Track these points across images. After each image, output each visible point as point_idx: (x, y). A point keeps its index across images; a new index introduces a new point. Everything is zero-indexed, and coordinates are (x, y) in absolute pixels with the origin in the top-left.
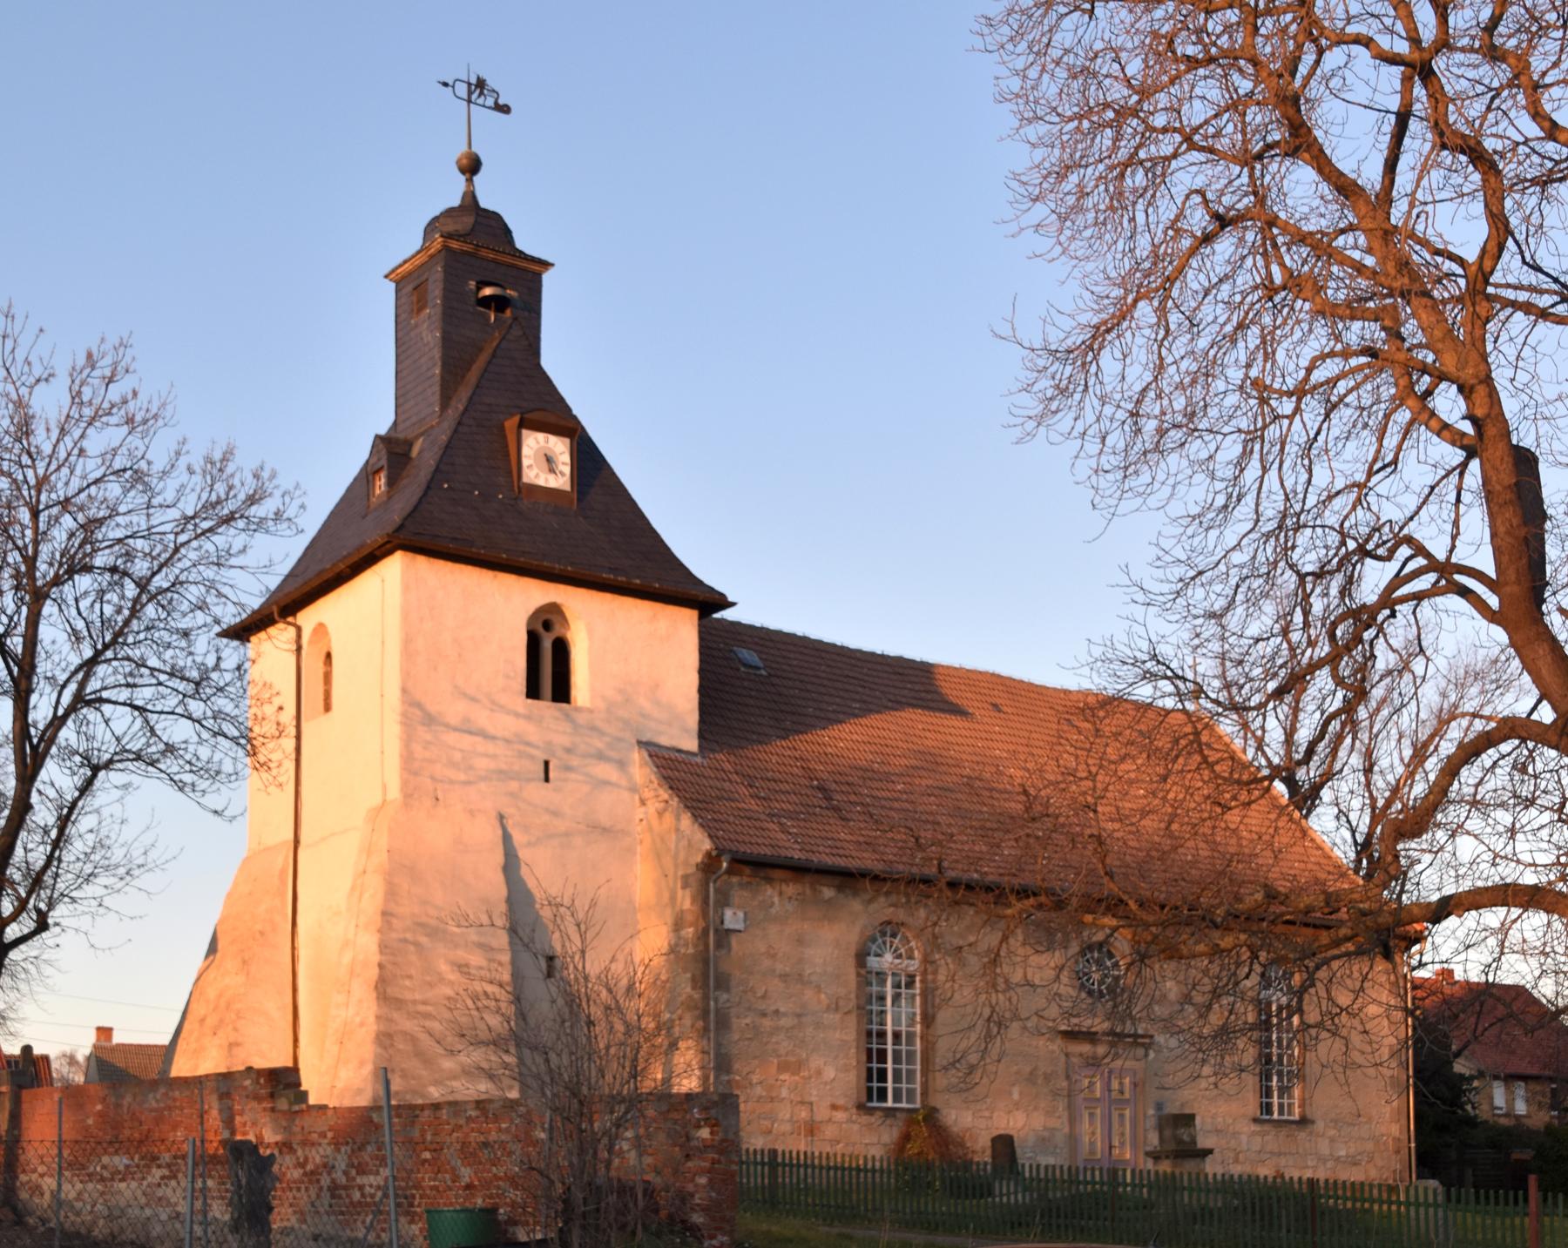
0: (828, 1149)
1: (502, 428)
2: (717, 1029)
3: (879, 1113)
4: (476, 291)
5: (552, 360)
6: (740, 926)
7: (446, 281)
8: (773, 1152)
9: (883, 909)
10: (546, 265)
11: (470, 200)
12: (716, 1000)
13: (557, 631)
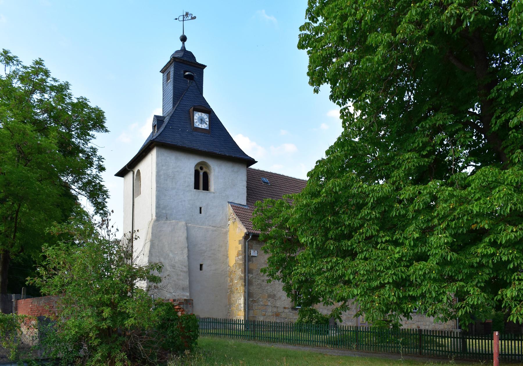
0: (283, 321)
1: (189, 111)
2: (248, 285)
4: (185, 73)
5: (206, 95)
6: (256, 255)
7: (174, 70)
8: (420, 331)
10: (205, 66)
11: (183, 49)
12: (248, 276)
13: (205, 170)
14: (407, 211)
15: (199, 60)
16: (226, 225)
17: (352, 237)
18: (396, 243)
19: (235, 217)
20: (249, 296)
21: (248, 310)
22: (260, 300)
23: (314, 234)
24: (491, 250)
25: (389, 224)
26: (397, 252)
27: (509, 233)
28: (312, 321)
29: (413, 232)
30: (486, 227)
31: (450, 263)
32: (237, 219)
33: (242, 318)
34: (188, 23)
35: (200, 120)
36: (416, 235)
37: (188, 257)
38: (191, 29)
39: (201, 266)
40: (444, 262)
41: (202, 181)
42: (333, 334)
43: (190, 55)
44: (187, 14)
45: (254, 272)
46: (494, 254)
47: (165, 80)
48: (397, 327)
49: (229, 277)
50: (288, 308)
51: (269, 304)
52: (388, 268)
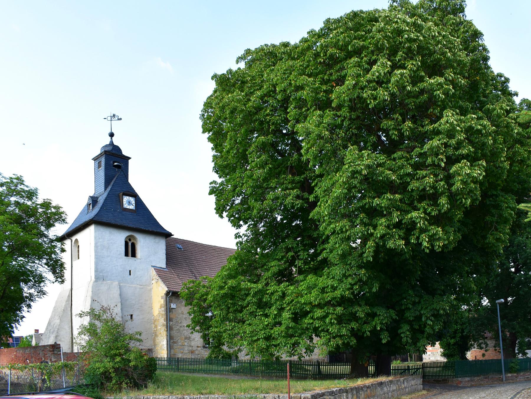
1: (119, 196)
4: (114, 163)
6: (175, 307)
10: (130, 158)
11: (112, 143)
13: (132, 241)
14: (271, 299)
15: (125, 153)
16: (150, 284)
17: (243, 311)
18: (266, 316)
19: (158, 278)
20: (171, 339)
21: (170, 349)
23: (222, 310)
24: (311, 321)
25: (262, 305)
26: (266, 321)
27: (318, 313)
28: (219, 356)
29: (274, 311)
30: (308, 310)
31: (291, 328)
32: (160, 280)
33: (166, 356)
34: (115, 123)
35: (128, 203)
36: (276, 312)
37: (121, 309)
38: (116, 127)
39: (131, 315)
40: (288, 328)
41: (130, 250)
42: (234, 365)
43: (117, 149)
44: (114, 116)
45: (173, 320)
46: (312, 323)
47: (97, 166)
48: (279, 359)
49: (154, 324)
50: (200, 347)
51: (186, 344)
52: (261, 330)
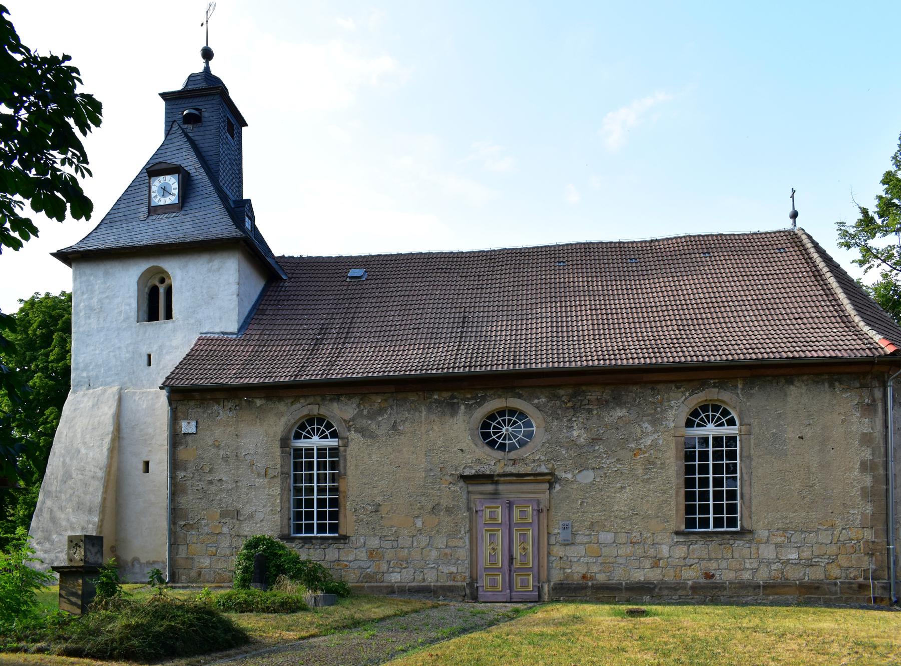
3: (298, 541)
6: (193, 430)
9: (303, 409)
22: (204, 522)
39: (147, 464)
45: (189, 465)
